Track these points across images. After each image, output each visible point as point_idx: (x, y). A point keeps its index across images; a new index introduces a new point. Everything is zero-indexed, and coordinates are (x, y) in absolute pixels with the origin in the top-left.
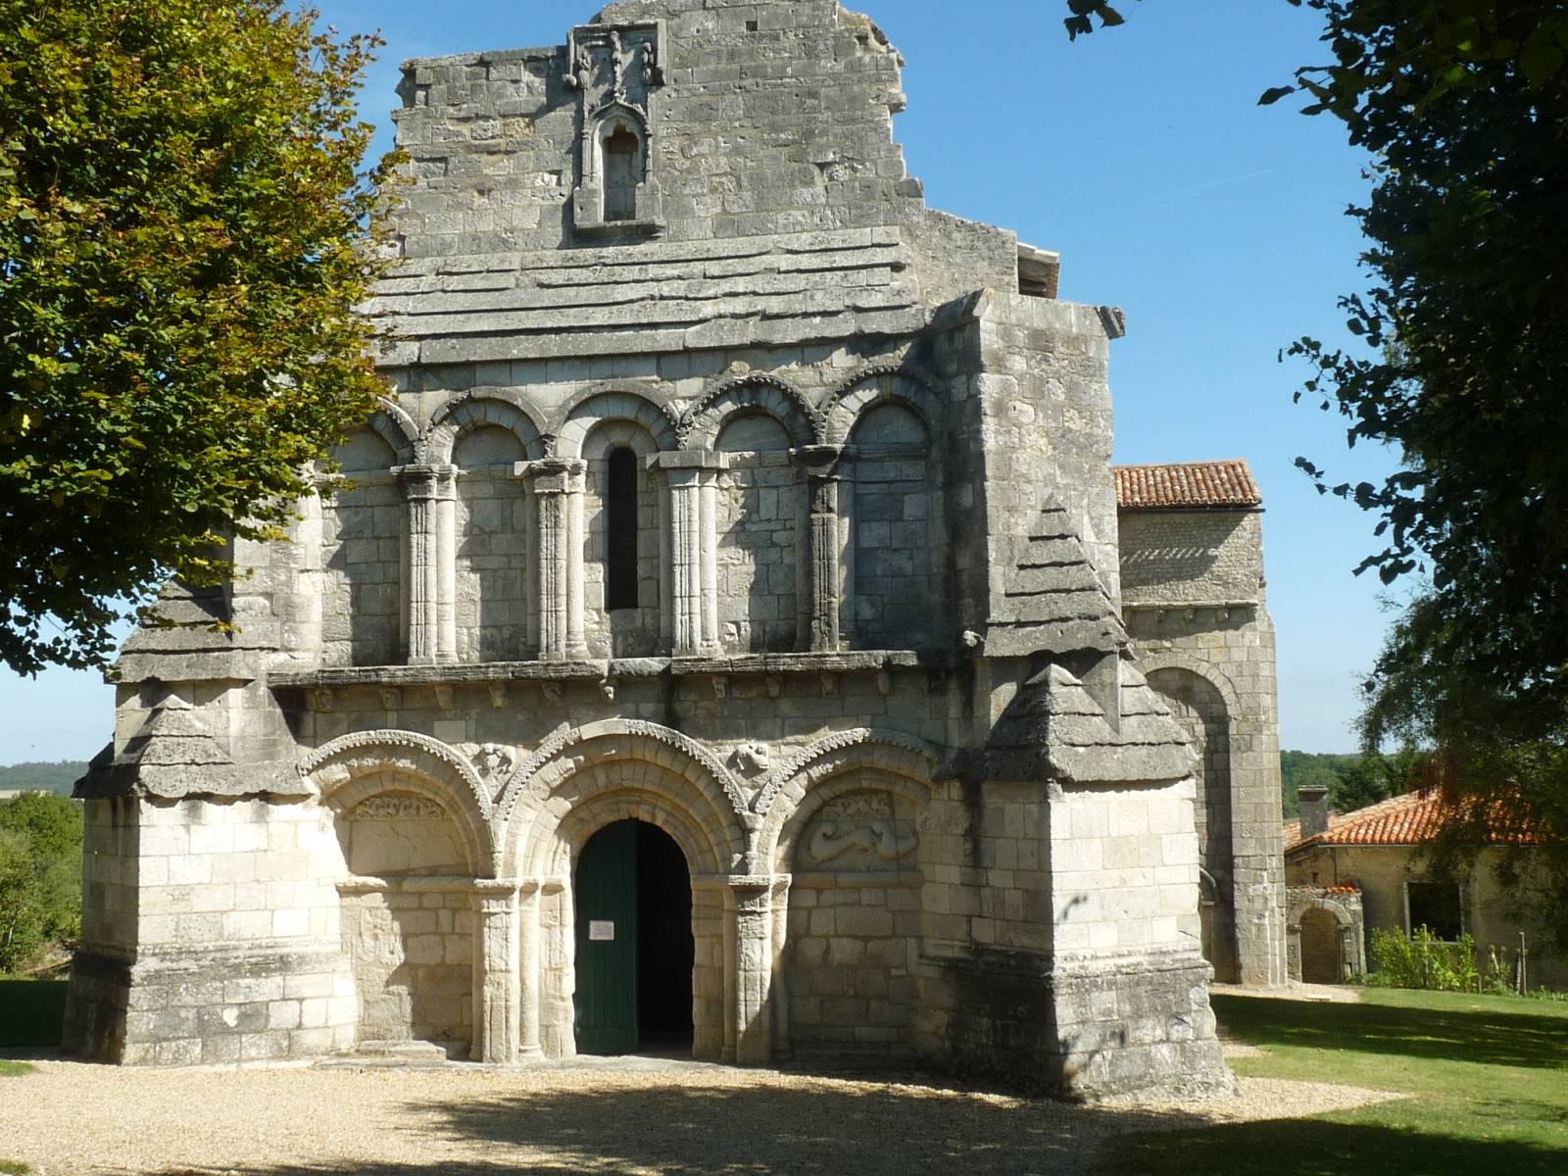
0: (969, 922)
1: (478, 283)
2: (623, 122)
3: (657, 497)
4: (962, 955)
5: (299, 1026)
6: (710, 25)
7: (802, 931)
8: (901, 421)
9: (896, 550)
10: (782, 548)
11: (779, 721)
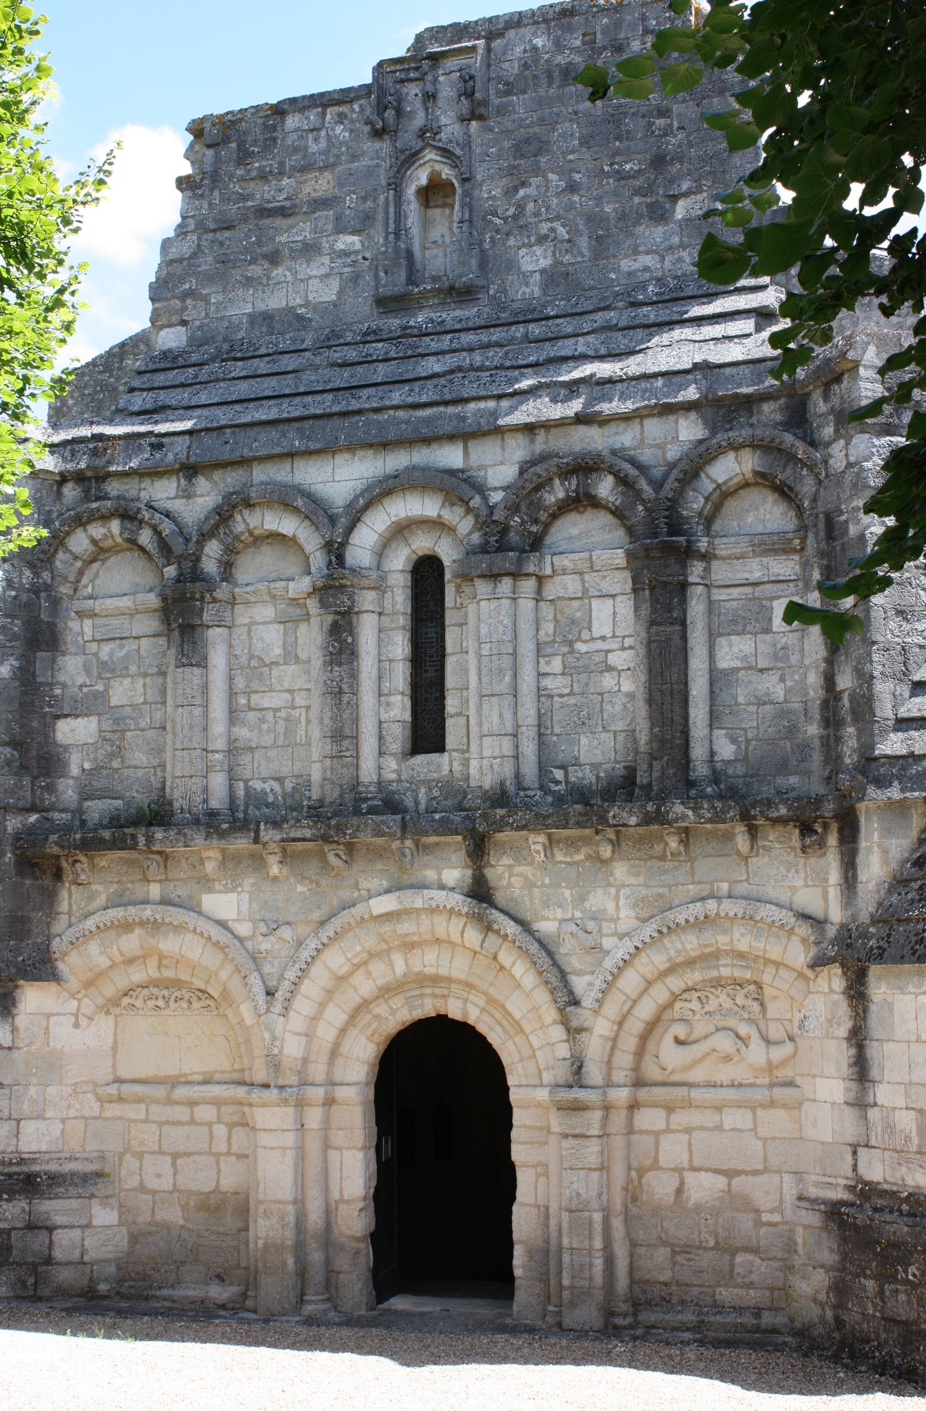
0: (855, 1153)
1: (262, 366)
2: (438, 167)
3: (466, 614)
4: (846, 1196)
5: (49, 1261)
6: (539, 42)
7: (648, 1162)
8: (768, 506)
9: (761, 671)
10: (619, 672)
11: (613, 890)
